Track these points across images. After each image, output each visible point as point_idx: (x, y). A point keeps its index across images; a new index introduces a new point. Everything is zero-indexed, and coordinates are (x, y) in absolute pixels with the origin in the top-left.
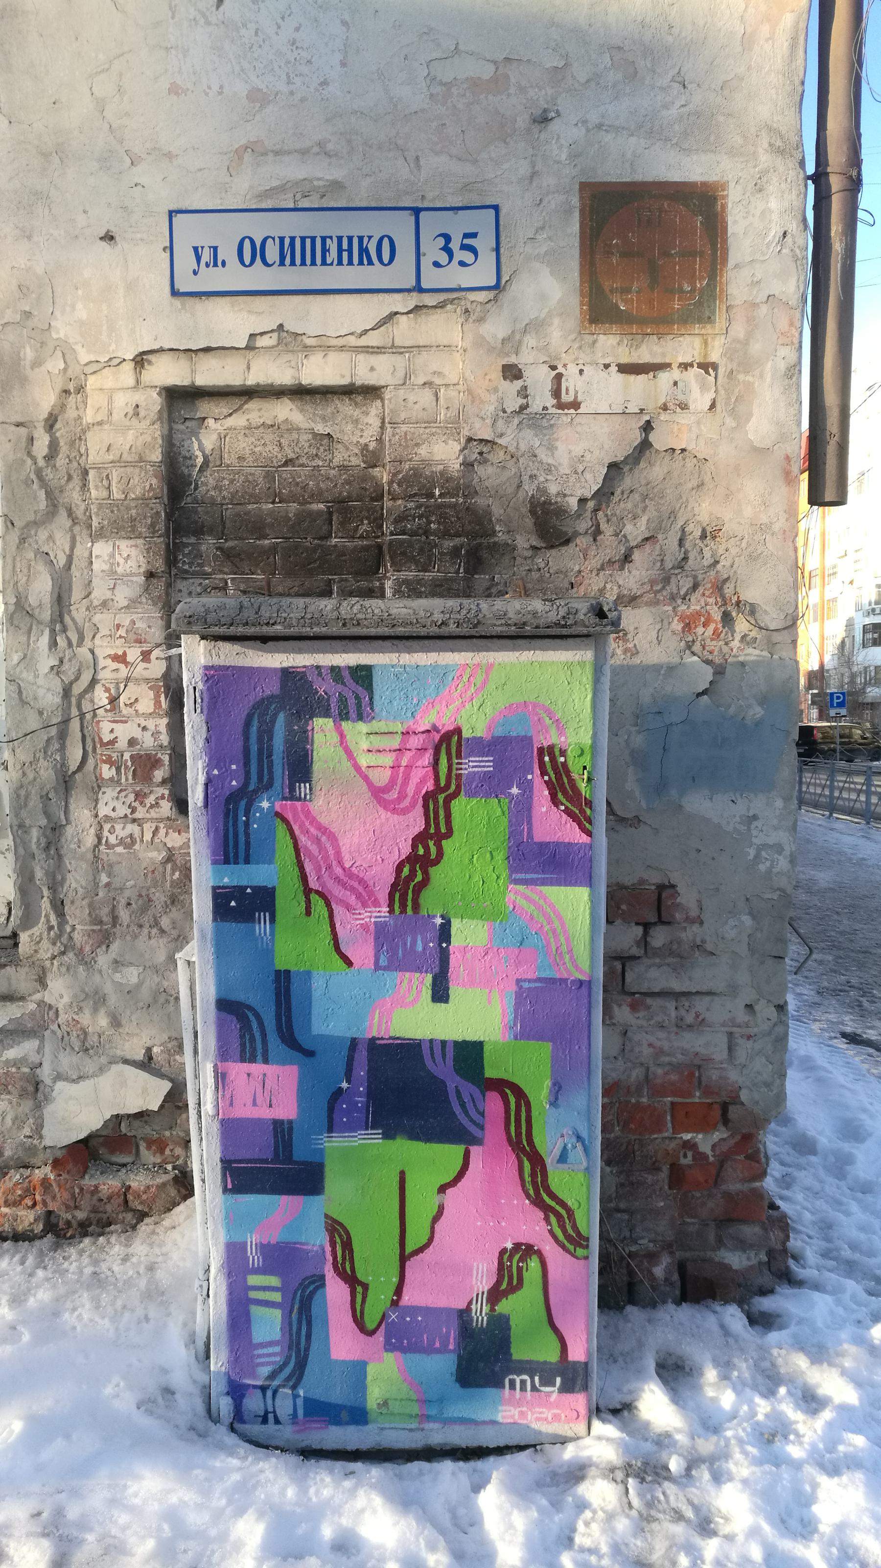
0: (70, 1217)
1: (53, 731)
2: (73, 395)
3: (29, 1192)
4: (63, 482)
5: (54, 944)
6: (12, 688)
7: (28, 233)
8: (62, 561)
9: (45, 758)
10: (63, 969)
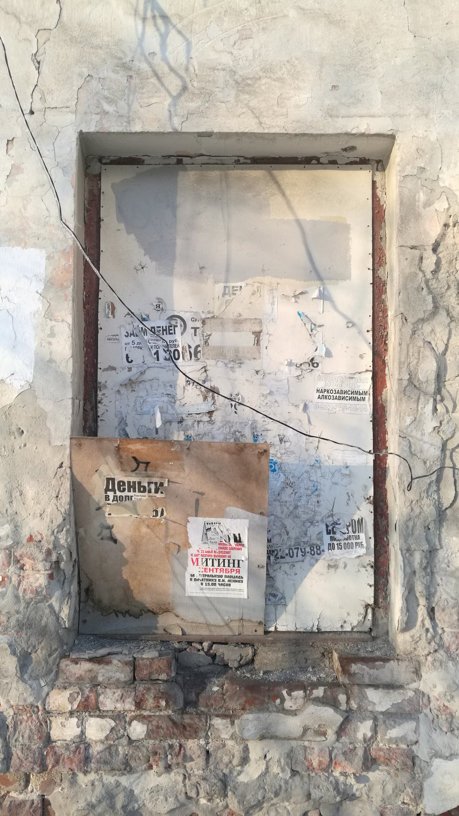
1: (434, 477)
2: (451, 228)
4: (443, 290)
5: (429, 643)
6: (405, 443)
8: (441, 348)
9: (427, 497)
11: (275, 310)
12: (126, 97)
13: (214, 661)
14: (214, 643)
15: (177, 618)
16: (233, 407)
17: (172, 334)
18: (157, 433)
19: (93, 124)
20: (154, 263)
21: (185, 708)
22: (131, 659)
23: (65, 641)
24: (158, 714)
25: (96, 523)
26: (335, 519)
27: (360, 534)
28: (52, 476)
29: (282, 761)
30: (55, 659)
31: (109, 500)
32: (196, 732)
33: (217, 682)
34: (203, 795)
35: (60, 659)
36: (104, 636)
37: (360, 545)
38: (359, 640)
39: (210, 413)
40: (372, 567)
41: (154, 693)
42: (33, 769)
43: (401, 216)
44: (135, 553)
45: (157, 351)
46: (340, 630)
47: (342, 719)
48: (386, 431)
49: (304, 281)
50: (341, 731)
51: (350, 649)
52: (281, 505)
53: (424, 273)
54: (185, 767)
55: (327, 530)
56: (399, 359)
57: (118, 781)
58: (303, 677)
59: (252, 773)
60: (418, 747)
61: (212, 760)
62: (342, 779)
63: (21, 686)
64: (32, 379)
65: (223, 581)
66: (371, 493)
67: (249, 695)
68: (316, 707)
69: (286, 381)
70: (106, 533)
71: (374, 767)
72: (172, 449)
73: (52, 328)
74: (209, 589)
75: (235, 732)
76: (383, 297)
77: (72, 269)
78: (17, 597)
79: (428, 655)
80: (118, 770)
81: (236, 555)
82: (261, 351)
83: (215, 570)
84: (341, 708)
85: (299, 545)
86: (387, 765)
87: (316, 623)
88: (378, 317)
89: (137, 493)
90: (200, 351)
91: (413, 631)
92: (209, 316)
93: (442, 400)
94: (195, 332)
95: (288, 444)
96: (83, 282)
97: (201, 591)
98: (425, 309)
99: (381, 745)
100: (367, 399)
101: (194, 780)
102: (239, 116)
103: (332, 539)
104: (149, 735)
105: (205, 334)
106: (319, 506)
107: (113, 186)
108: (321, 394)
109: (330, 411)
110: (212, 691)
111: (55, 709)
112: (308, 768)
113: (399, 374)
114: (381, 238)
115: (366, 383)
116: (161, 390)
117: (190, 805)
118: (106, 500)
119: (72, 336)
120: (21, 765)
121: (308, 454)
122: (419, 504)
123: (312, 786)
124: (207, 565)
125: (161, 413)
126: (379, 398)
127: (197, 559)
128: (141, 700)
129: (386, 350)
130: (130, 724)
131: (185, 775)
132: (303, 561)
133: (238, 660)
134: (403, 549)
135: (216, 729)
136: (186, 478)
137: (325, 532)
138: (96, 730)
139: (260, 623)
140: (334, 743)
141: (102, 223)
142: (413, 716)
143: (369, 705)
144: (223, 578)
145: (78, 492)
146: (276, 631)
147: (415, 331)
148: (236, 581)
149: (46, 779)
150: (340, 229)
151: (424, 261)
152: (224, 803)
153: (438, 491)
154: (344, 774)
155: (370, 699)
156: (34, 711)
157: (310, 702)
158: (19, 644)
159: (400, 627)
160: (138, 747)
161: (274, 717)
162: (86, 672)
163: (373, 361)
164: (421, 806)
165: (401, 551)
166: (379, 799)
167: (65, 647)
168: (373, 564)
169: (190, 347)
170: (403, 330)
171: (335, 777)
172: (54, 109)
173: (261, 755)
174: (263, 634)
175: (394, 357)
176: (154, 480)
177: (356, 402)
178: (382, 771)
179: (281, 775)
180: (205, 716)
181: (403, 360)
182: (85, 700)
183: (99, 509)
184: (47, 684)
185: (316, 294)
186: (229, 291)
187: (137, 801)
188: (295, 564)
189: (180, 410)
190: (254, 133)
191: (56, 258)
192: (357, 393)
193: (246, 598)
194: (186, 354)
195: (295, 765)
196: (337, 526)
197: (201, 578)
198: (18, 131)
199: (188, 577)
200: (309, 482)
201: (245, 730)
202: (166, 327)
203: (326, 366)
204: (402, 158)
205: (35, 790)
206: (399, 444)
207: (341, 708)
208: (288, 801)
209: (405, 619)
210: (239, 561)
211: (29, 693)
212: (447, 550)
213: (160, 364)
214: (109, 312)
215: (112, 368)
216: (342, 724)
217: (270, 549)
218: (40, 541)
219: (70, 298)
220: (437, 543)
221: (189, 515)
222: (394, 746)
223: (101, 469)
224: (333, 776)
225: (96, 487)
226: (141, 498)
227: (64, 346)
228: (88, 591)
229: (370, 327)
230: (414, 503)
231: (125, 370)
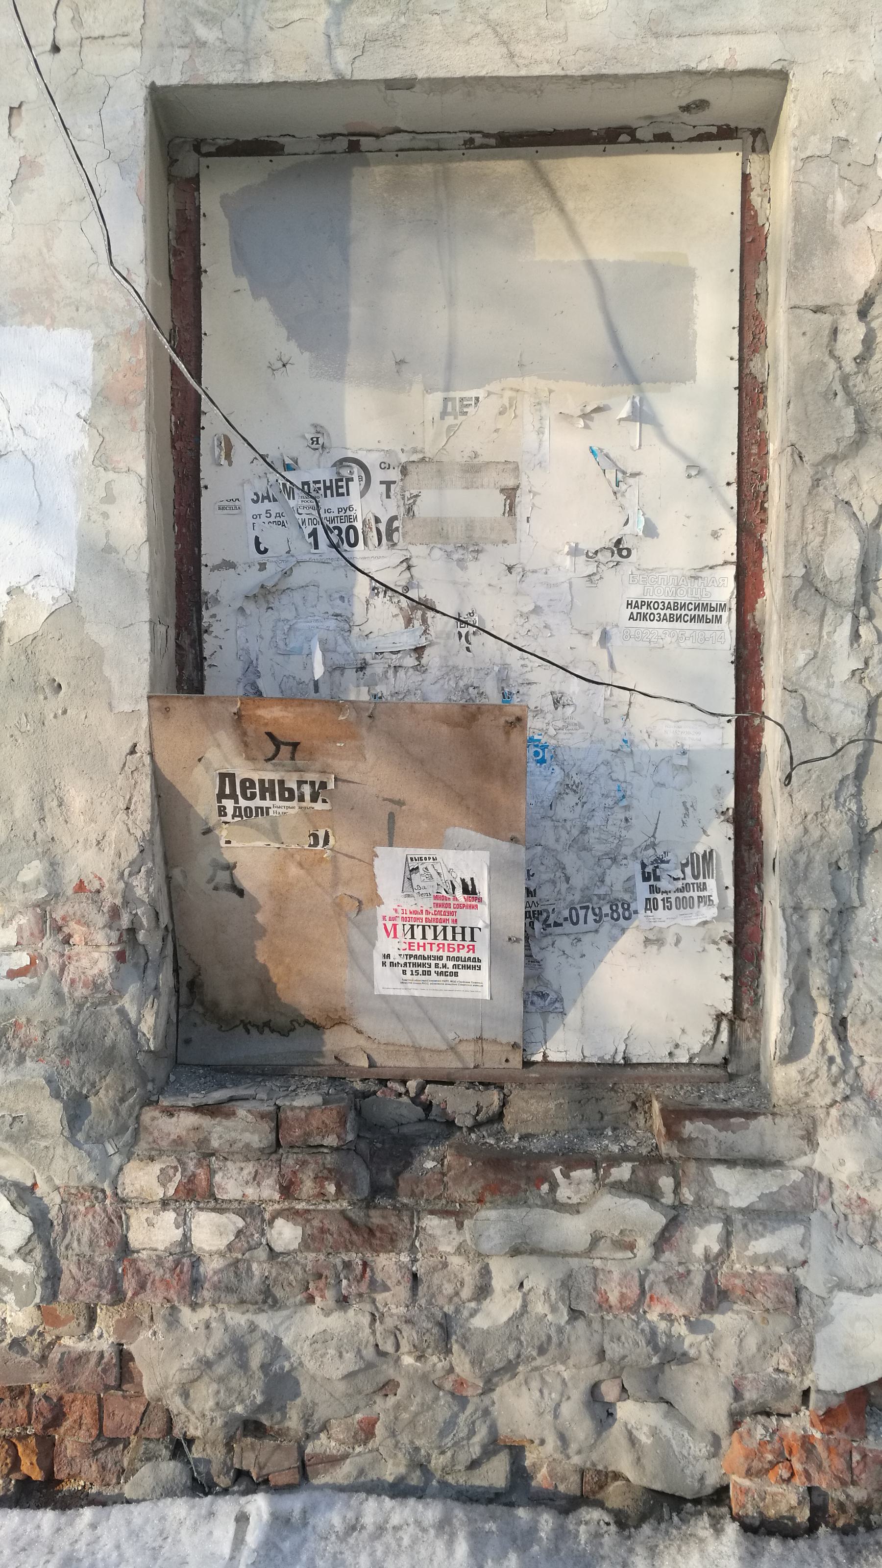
0: (843, 1498)
3: (782, 1457)
5: (834, 1084)
6: (793, 702)
7: (851, 22)
9: (836, 808)
10: (848, 1122)
11: (546, 444)
12: (239, 11)
13: (427, 1115)
14: (428, 1082)
15: (359, 1036)
16: (463, 638)
17: (343, 494)
18: (317, 690)
19: (177, 67)
20: (307, 354)
21: (373, 1198)
22: (272, 1108)
23: (150, 1075)
24: (322, 1207)
25: (204, 860)
26: (660, 852)
27: (707, 881)
28: (117, 769)
29: (553, 1293)
30: (132, 1107)
31: (225, 815)
32: (392, 1241)
33: (433, 1153)
34: (406, 1350)
35: (141, 1108)
36: (224, 1069)
37: (706, 901)
38: (702, 1079)
39: (419, 651)
40: (729, 942)
41: (313, 1170)
42: (99, 1296)
43: (796, 244)
44: (279, 915)
45: (315, 530)
46: (668, 1060)
47: (664, 1221)
48: (762, 681)
49: (603, 385)
50: (663, 1241)
51: (684, 1095)
52: (556, 827)
53: (839, 362)
54: (374, 1301)
55: (643, 873)
56: (786, 537)
57: (252, 1323)
58: (594, 1146)
59: (498, 1311)
60: (808, 1272)
61: (422, 1289)
62: (663, 1325)
63: (72, 1153)
64: (73, 583)
65: (445, 966)
66: (730, 801)
67: (491, 1175)
68: (616, 1199)
69: (567, 585)
70: (223, 877)
71: (725, 1305)
72: (341, 718)
73: (108, 486)
74: (418, 982)
75: (465, 1241)
76: (760, 414)
77: (143, 368)
78: (58, 994)
79: (831, 1106)
80: (252, 1304)
81: (466, 918)
82: (518, 526)
83: (428, 947)
84: (663, 1200)
85: (590, 901)
86: (748, 1302)
87: (622, 1048)
88: (750, 455)
89: (278, 802)
90: (397, 529)
91: (804, 1062)
92: (415, 457)
93: (870, 617)
94: (388, 490)
95: (569, 710)
96: (169, 396)
97: (402, 986)
98: (839, 435)
99: (737, 1266)
100: (724, 619)
101: (390, 1322)
102: (467, 42)
103: (653, 889)
104: (306, 1244)
105: (407, 494)
106: (627, 828)
107: (224, 201)
108: (635, 611)
109: (652, 645)
110: (423, 1168)
111: (134, 1194)
112: (600, 1306)
113: (786, 565)
114: (758, 294)
115: (724, 588)
116: (324, 606)
117: (385, 1367)
118: (220, 815)
119: (147, 501)
120: (77, 1290)
121: (608, 729)
122: (820, 820)
123: (607, 1338)
124: (413, 937)
125: (324, 651)
126: (749, 617)
127: (395, 926)
128: (291, 1183)
129: (764, 522)
130: (271, 1223)
131: (373, 1315)
132: (597, 931)
133: (474, 1112)
134: (786, 905)
135: (430, 1235)
136: (370, 771)
137: (639, 877)
138: (210, 1233)
139: (515, 1046)
140: (650, 1263)
141: (203, 278)
142: (799, 1217)
143: (717, 1197)
144: (444, 961)
145: (166, 799)
146: (546, 1062)
147: (818, 480)
148: (469, 967)
149: (124, 1316)
150: (675, 277)
151: (840, 337)
152: (445, 1364)
153: (858, 794)
154: (668, 1318)
155: (719, 1185)
156: (96, 1198)
157: (604, 1190)
158: (65, 1080)
159: (778, 1053)
160: (287, 1264)
161: (536, 1215)
162: (188, 1130)
163: (739, 544)
164: (811, 1376)
165: (783, 910)
166: (732, 1362)
167: (150, 1087)
168: (731, 938)
169: (377, 520)
170: (795, 478)
171: (649, 1322)
172: (99, 40)
173: (513, 1281)
174: (520, 1066)
175: (777, 533)
176: (309, 777)
177: (703, 626)
178: (738, 1313)
179: (550, 1317)
180: (408, 1213)
181: (792, 537)
182: (189, 1181)
183: (208, 831)
184: (119, 1151)
185: (625, 410)
186: (454, 408)
187: (288, 1358)
188: (580, 936)
189: (360, 645)
190: (498, 79)
191: (113, 346)
192: (705, 607)
193: (488, 998)
194: (370, 535)
195: (578, 1301)
196: (663, 866)
197: (402, 961)
198: (31, 89)
199: (378, 960)
200: (610, 782)
201: (483, 1238)
202: (331, 481)
203: (645, 554)
204: (800, 121)
205: (105, 1335)
206: (783, 704)
207: (663, 1200)
208: (563, 1363)
209: (789, 1039)
210: (472, 929)
211: (86, 1166)
212: (874, 909)
213: (321, 555)
214: (220, 455)
215: (229, 565)
216: (665, 1229)
217: (533, 908)
218: (98, 892)
219: (142, 426)
220: (854, 896)
221: (376, 844)
222: (762, 1269)
223: (208, 755)
224: (646, 1320)
225: (201, 792)
226: (285, 810)
227: (131, 520)
228: (193, 985)
229: (733, 476)
230: (809, 817)
231: (253, 568)
